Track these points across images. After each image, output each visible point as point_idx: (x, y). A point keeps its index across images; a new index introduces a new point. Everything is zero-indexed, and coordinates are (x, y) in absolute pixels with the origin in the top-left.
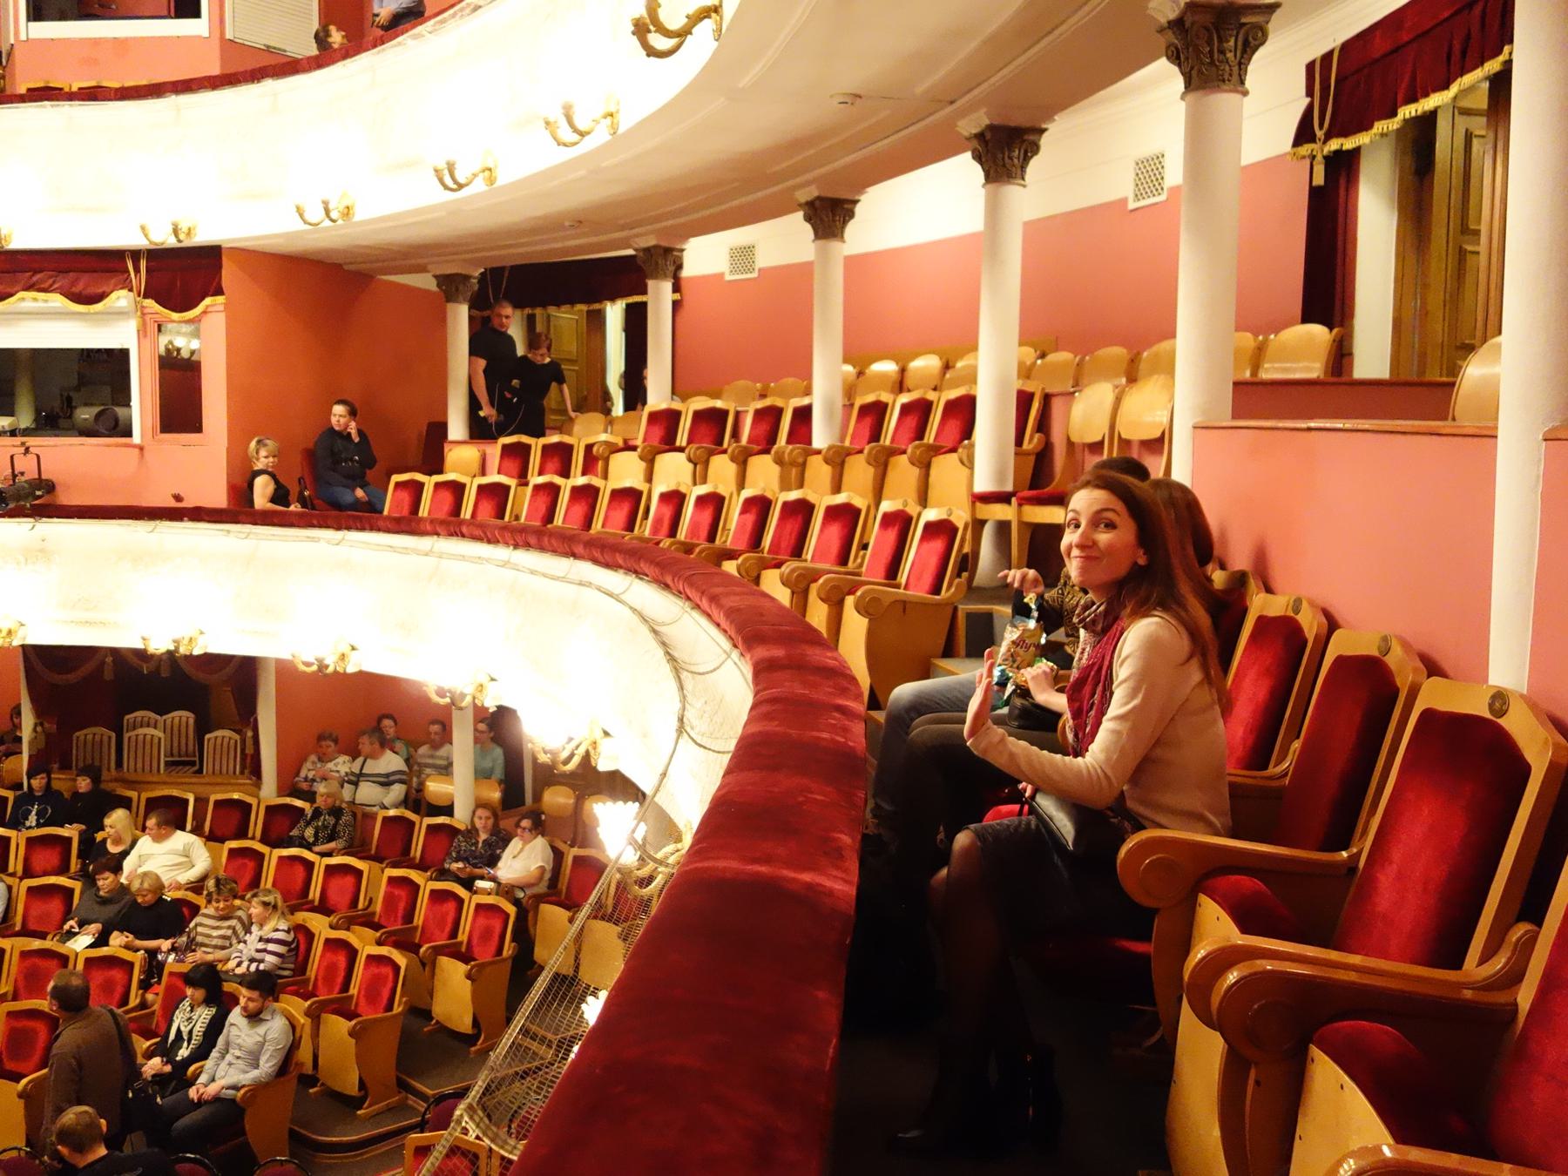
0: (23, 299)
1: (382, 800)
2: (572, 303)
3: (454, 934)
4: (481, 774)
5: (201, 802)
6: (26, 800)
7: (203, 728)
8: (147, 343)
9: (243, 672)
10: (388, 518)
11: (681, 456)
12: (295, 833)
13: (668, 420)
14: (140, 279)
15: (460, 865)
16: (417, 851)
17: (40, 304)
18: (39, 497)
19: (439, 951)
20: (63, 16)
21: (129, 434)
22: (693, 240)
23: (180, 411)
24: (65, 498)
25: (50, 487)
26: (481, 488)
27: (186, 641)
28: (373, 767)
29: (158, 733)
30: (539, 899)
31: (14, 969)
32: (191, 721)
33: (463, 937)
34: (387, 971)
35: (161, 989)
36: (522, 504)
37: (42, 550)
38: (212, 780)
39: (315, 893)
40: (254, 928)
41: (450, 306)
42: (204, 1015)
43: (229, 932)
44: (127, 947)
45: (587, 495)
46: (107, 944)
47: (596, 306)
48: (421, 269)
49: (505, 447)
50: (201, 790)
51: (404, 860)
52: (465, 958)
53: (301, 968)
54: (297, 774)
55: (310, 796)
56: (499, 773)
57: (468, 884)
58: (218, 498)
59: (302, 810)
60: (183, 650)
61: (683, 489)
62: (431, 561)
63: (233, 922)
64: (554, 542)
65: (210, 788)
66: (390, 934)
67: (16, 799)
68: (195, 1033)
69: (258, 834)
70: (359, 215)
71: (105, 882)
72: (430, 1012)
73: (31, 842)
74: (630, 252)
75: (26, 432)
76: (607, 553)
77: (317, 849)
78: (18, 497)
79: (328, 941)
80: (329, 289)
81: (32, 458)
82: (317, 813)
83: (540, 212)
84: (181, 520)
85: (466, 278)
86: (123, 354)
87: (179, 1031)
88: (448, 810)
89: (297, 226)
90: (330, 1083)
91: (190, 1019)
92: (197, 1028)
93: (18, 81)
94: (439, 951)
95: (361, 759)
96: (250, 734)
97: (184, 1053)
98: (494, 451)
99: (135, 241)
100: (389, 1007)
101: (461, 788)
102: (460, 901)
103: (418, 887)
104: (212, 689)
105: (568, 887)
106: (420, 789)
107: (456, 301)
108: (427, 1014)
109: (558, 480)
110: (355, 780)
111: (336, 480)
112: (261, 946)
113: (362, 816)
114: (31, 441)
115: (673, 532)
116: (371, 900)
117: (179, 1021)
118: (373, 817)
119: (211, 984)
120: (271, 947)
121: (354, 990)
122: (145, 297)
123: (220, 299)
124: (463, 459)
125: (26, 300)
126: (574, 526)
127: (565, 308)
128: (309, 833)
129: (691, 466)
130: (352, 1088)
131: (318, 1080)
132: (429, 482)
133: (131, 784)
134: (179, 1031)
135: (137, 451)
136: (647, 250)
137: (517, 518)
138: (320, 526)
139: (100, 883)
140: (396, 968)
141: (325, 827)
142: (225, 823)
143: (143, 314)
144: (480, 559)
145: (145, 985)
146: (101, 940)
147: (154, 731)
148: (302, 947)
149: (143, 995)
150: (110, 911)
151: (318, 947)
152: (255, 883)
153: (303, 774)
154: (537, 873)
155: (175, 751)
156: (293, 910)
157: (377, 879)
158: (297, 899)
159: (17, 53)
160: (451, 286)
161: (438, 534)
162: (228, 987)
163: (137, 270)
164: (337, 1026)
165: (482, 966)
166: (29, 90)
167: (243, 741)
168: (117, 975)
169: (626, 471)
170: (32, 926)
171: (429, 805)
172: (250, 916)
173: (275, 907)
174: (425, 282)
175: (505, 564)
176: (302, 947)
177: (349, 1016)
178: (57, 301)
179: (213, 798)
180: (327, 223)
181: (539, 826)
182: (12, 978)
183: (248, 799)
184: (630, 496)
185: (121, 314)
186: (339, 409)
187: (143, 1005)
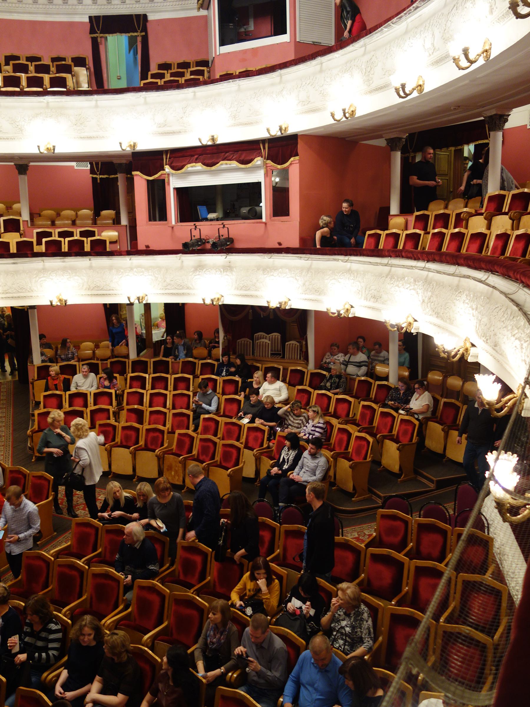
0: (222, 164)
1: (358, 373)
2: (447, 146)
3: (391, 430)
4: (401, 364)
5: (285, 370)
6: (221, 365)
7: (284, 340)
8: (268, 179)
9: (301, 316)
10: (365, 250)
11: (506, 217)
12: (322, 384)
13: (498, 200)
14: (265, 152)
15: (393, 403)
16: (373, 394)
17: (228, 166)
18: (229, 245)
19: (385, 437)
20: (232, 42)
21: (261, 218)
22: (515, 110)
23: (281, 208)
24: (238, 245)
25: (231, 240)
26: (407, 235)
27: (283, 304)
28: (354, 359)
29: (267, 341)
30: (427, 419)
31: (222, 429)
32: (279, 337)
33: (395, 432)
34: (365, 443)
35: (275, 442)
36: (426, 242)
37: (229, 267)
38: (288, 361)
39: (332, 409)
40: (310, 421)
41: (392, 153)
42: (292, 454)
43: (300, 422)
44: (262, 424)
45: (458, 237)
46: (254, 423)
47: (459, 147)
48: (380, 137)
49: (417, 216)
50: (286, 365)
51: (367, 398)
52: (396, 441)
53: (328, 439)
54: (322, 361)
55: (329, 370)
56: (407, 364)
57: (396, 410)
58: (295, 243)
59: (325, 375)
60: (283, 307)
61: (509, 232)
62: (387, 268)
63: (302, 418)
64: (448, 258)
65: (288, 364)
66: (364, 428)
67: (218, 365)
68: (290, 460)
69: (307, 384)
70: (358, 114)
71: (253, 398)
72: (381, 462)
73: (225, 381)
74: (482, 118)
75: (222, 219)
76: (476, 262)
77: (332, 391)
78: (222, 245)
79: (339, 429)
80: (341, 150)
81: (226, 229)
82: (331, 377)
83: (440, 104)
84: (282, 253)
85: (400, 139)
86: (259, 184)
87: (284, 458)
88: (386, 378)
89: (37, 152)
90: (341, 486)
91: (287, 455)
92: (290, 458)
93: (216, 71)
94: (385, 437)
95: (348, 355)
96: (304, 343)
97: (286, 467)
98: (412, 219)
99: (262, 134)
100: (365, 458)
101: (392, 369)
102: (394, 417)
103: (375, 410)
104: (288, 323)
105: (441, 416)
106: (374, 368)
107: (396, 150)
108: (379, 463)
109: (444, 230)
110: (346, 363)
111: (344, 234)
112: (313, 429)
113: (350, 379)
114: (225, 222)
115: (503, 252)
116: (355, 414)
117: (284, 454)
118: (354, 380)
119: (295, 442)
120: (317, 429)
121: (350, 450)
123: (297, 158)
124: (397, 222)
125: (223, 164)
126: (452, 251)
127: (444, 149)
128: (328, 384)
129: (511, 221)
130: (350, 487)
131: (336, 484)
132: (383, 234)
133: (258, 361)
134: (284, 458)
135: (264, 225)
136: (491, 117)
137: (424, 248)
138: (338, 254)
139: (251, 399)
140: (368, 442)
141: (335, 383)
142: (294, 379)
143: (267, 167)
144: (412, 267)
145: (269, 440)
146: (252, 421)
147: (267, 340)
148: (329, 430)
149: (268, 443)
150: (255, 410)
151: (335, 431)
152: (308, 403)
153: (324, 361)
154: (425, 407)
155: (273, 349)
156: (325, 415)
157: (358, 407)
158: (326, 412)
159: (216, 61)
160: (393, 144)
161: (391, 257)
162: (301, 443)
163: (264, 148)
164: (344, 464)
165: (404, 446)
166: (221, 76)
167: (301, 346)
168: (259, 434)
169: (477, 225)
170: (227, 413)
171: (377, 376)
172: (308, 416)
173: (318, 413)
174: (381, 143)
175: (423, 269)
176: (329, 430)
177: (349, 460)
178: (234, 164)
179: (290, 368)
180: (344, 119)
181: (426, 387)
182: (222, 432)
183: (304, 370)
184: (481, 237)
185: (258, 167)
186: (345, 205)
187: (269, 447)
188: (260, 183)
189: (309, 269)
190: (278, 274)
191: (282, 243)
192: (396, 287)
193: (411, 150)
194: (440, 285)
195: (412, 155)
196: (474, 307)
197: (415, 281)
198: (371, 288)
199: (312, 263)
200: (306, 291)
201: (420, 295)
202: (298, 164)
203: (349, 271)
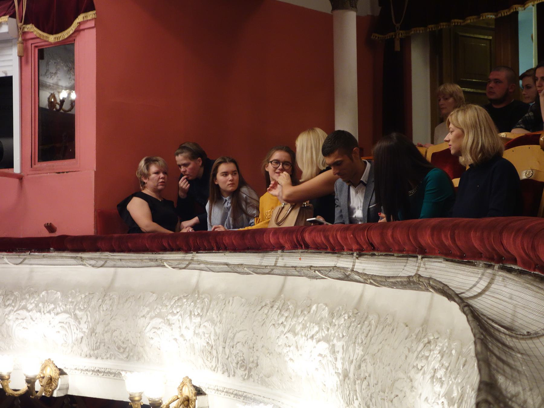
21: (11, 166)
24: (437, 129)
47: (505, 13)
58: (84, 224)
62: (275, 281)
84: (48, 251)
122: (26, 23)
123: (91, 15)
135: (17, 181)
143: (25, 41)
161: (282, 248)
188: (11, 78)
189: (107, 291)
190: (37, 306)
191: (55, 225)
192: (289, 335)
193: (398, 25)
194: (386, 322)
195: (401, 34)
196: (455, 394)
197: (332, 314)
198: (236, 340)
199: (115, 273)
200: (98, 348)
201: (339, 356)
202: (94, 31)
203: (194, 293)
